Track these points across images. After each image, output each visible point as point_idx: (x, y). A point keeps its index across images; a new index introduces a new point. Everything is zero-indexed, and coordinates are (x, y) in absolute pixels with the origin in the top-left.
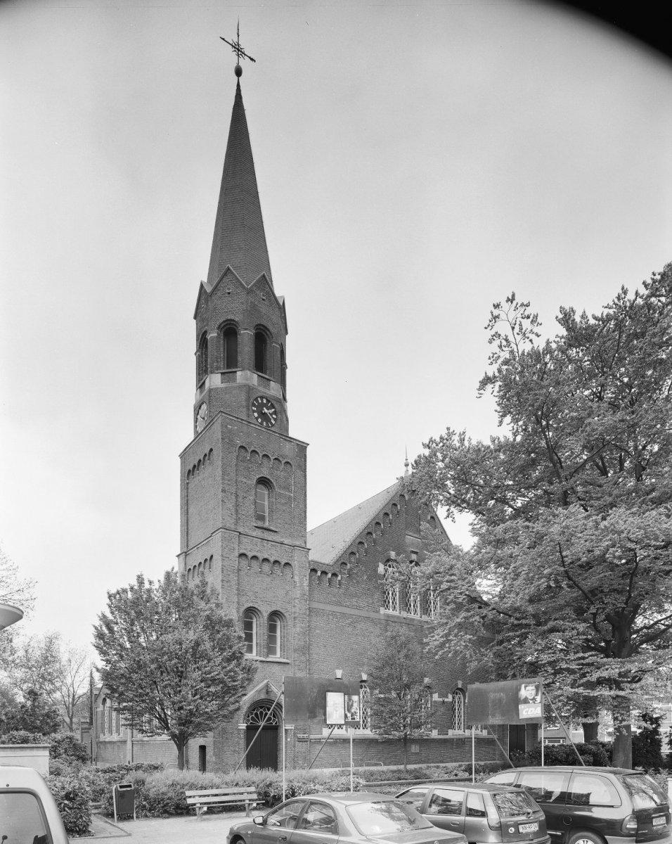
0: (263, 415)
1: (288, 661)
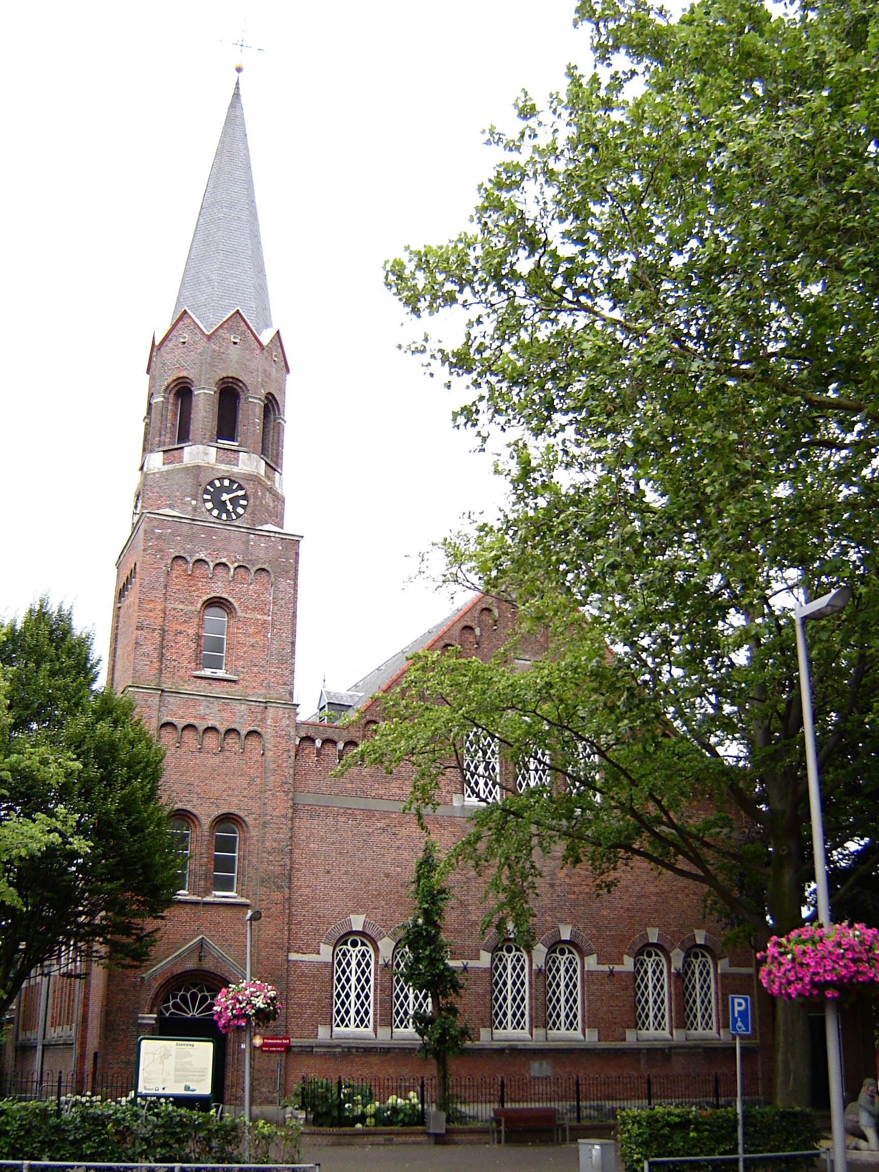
0: (221, 506)
1: (248, 901)
